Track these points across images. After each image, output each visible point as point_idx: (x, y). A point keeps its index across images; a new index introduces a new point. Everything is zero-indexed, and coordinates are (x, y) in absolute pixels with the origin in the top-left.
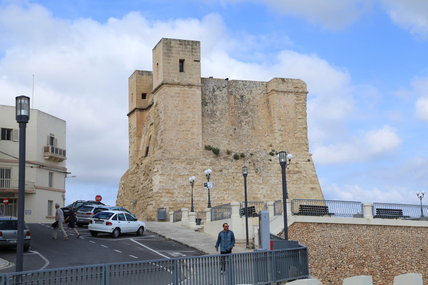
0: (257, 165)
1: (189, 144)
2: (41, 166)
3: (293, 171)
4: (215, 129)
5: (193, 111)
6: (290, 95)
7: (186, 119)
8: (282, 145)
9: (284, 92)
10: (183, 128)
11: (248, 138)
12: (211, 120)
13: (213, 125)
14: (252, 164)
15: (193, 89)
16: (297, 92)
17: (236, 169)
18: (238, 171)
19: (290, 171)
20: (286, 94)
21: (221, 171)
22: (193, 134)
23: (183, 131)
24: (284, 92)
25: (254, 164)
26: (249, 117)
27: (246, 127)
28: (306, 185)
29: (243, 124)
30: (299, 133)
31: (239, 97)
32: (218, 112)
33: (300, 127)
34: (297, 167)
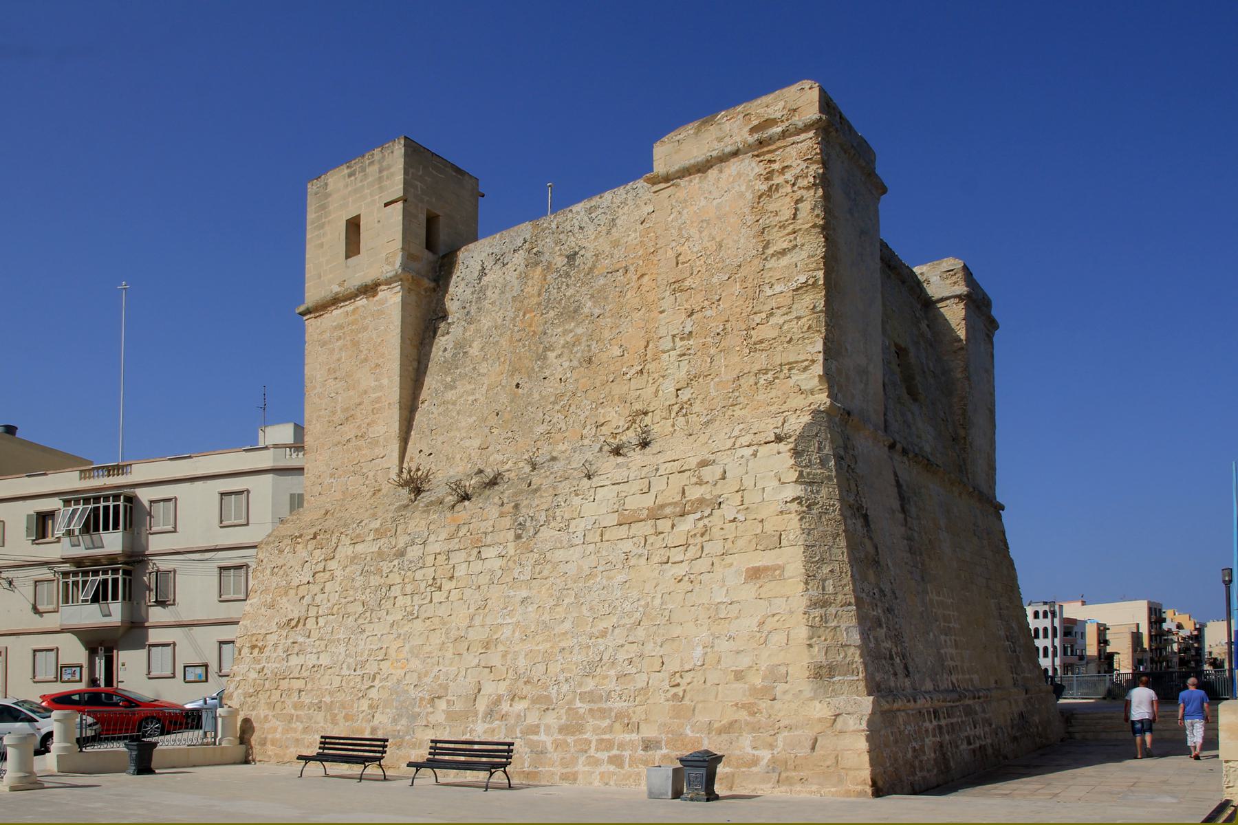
0: (526, 506)
1: (361, 480)
2: (491, 774)
3: (675, 504)
4: (450, 407)
5: (377, 365)
6: (733, 166)
7: (357, 401)
8: (685, 395)
9: (702, 168)
10: (349, 431)
11: (557, 407)
12: (449, 379)
13: (450, 395)
14: (508, 507)
15: (381, 295)
16: (761, 143)
17: (451, 537)
18: (454, 544)
19: (662, 507)
20: (713, 173)
21: (402, 554)
22: (375, 443)
23: (349, 441)
24: (702, 168)
25: (516, 507)
26: (578, 325)
27: (558, 365)
28: (728, 559)
29: (551, 355)
30: (773, 321)
31: (560, 261)
32: (475, 344)
33: (778, 288)
34: (700, 483)
